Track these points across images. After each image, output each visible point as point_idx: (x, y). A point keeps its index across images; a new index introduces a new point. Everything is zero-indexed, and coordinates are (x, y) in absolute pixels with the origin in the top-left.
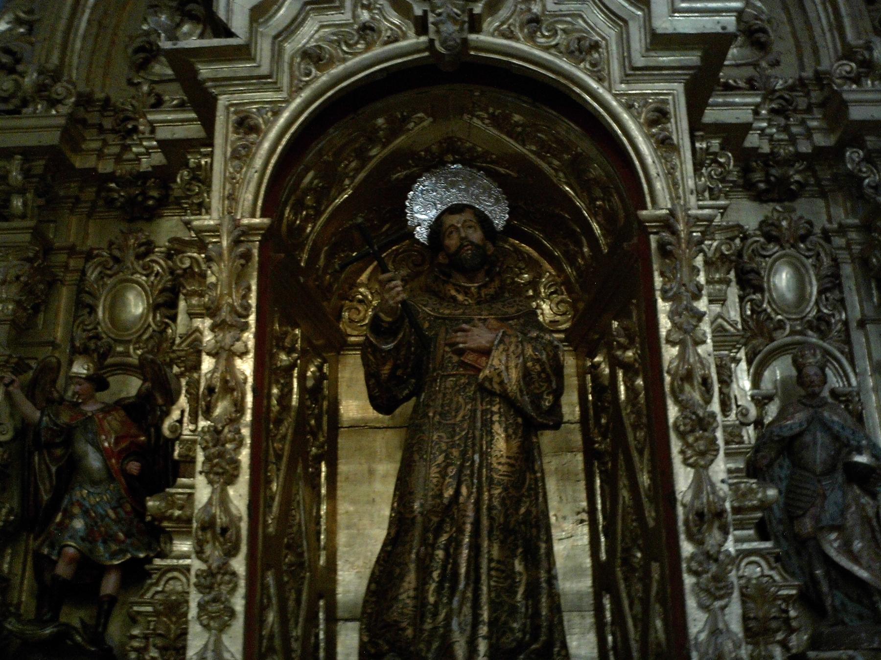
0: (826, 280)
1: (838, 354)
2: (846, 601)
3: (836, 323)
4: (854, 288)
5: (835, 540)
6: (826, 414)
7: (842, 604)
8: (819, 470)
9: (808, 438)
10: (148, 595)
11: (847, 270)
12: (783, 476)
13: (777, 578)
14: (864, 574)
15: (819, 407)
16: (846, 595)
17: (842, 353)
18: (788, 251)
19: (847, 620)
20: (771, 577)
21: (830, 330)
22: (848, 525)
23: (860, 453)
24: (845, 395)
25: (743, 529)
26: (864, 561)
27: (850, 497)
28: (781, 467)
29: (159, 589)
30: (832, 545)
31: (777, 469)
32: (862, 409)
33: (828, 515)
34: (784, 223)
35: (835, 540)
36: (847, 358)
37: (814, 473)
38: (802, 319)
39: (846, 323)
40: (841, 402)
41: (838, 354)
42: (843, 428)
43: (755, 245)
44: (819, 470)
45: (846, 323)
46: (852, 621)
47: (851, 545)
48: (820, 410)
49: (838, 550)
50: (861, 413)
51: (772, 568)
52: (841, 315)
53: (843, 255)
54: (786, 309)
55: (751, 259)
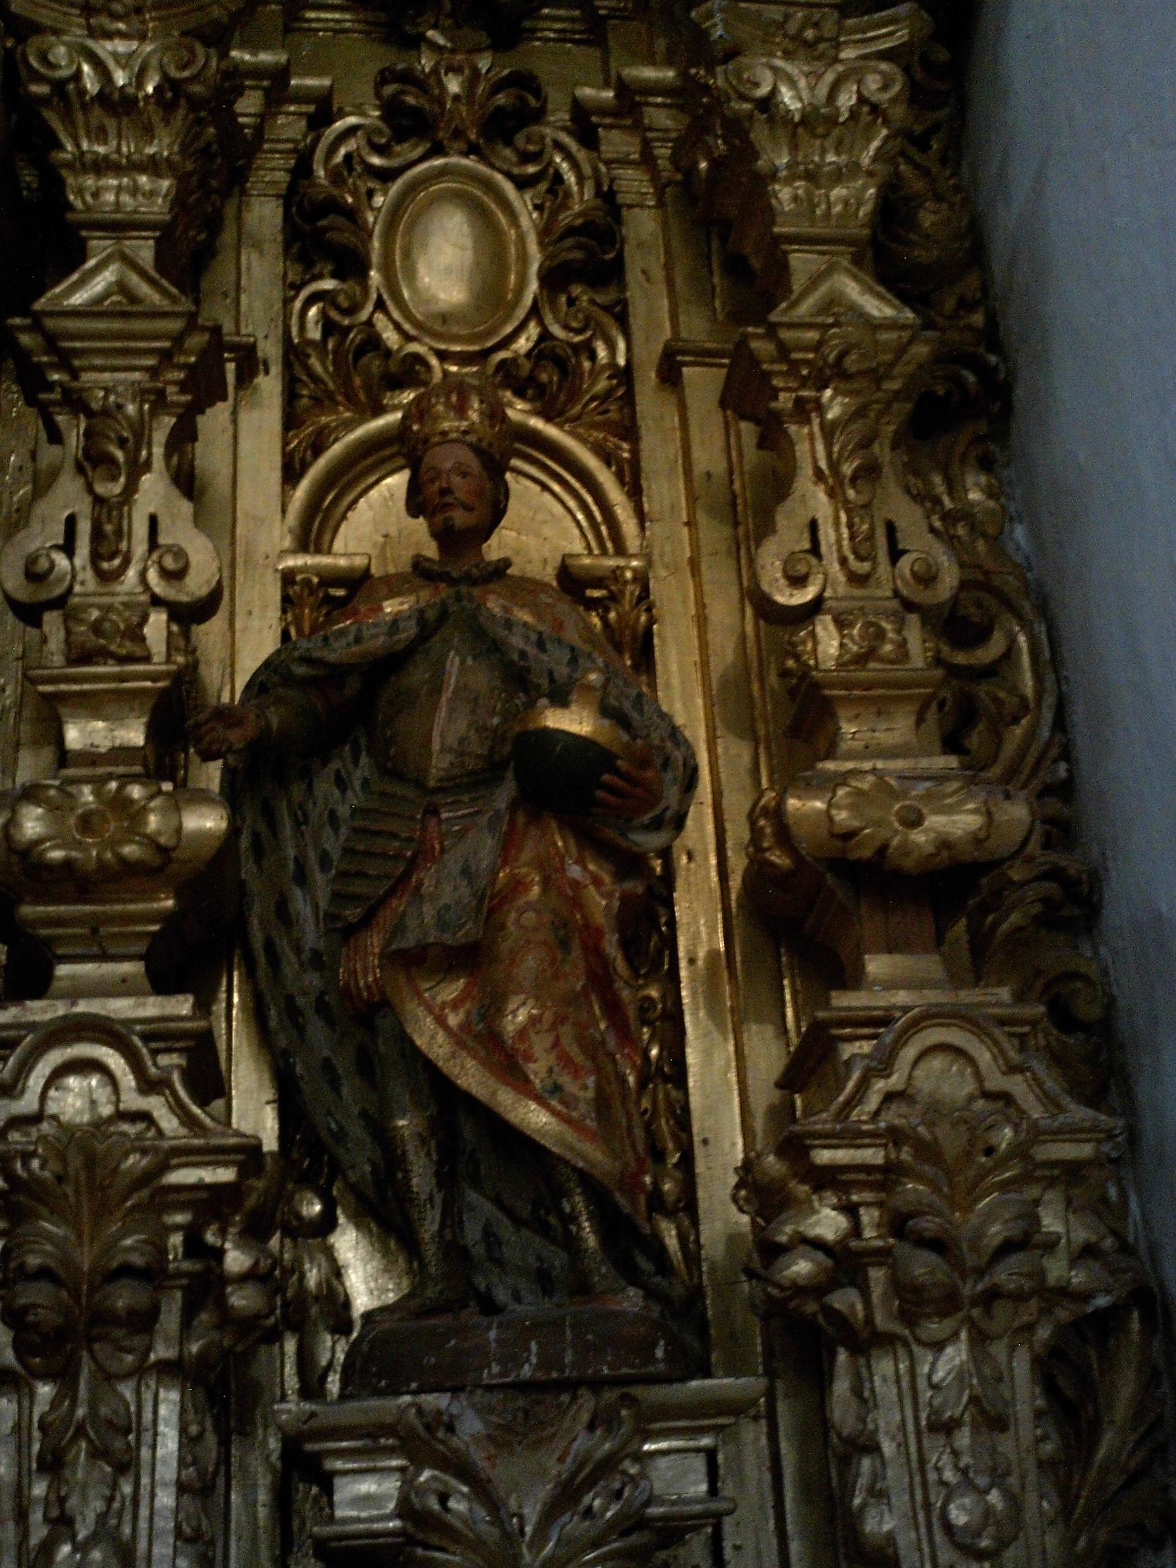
0: (569, 242)
1: (591, 462)
2: (505, 1229)
3: (594, 374)
4: (658, 273)
5: (455, 1005)
6: (494, 605)
7: (490, 1236)
8: (439, 764)
9: (417, 675)
10: (862, 1113)
11: (643, 226)
12: (343, 811)
13: (169, 1123)
14: (536, 1118)
15: (473, 582)
16: (498, 1201)
17: (607, 458)
18: (454, 160)
19: (501, 1295)
20: (144, 1117)
21: (574, 395)
22: (505, 946)
23: (560, 699)
24: (598, 583)
25: (104, 957)
26: (537, 1070)
27: (527, 854)
28: (342, 783)
29: (895, 1081)
30: (433, 1025)
31: (324, 786)
32: (652, 621)
33: (429, 912)
34: (453, 85)
35: (455, 1005)
36: (620, 476)
37: (420, 785)
38: (486, 354)
39: (626, 375)
40: (591, 604)
41: (591, 462)
42: (541, 645)
43: (350, 146)
44: (439, 764)
45: (626, 375)
46: (517, 1298)
47: (500, 1011)
48: (476, 592)
49: (459, 1039)
50: (648, 634)
51: (147, 1086)
52: (612, 348)
53: (633, 183)
54: (438, 327)
55: (336, 177)
